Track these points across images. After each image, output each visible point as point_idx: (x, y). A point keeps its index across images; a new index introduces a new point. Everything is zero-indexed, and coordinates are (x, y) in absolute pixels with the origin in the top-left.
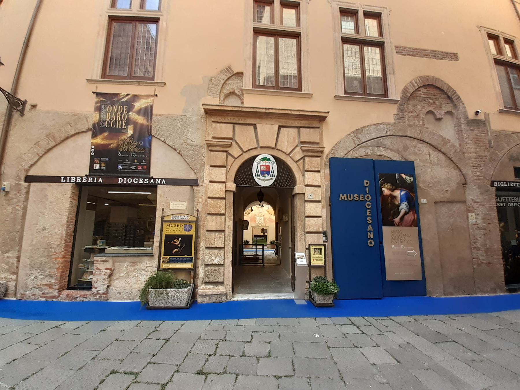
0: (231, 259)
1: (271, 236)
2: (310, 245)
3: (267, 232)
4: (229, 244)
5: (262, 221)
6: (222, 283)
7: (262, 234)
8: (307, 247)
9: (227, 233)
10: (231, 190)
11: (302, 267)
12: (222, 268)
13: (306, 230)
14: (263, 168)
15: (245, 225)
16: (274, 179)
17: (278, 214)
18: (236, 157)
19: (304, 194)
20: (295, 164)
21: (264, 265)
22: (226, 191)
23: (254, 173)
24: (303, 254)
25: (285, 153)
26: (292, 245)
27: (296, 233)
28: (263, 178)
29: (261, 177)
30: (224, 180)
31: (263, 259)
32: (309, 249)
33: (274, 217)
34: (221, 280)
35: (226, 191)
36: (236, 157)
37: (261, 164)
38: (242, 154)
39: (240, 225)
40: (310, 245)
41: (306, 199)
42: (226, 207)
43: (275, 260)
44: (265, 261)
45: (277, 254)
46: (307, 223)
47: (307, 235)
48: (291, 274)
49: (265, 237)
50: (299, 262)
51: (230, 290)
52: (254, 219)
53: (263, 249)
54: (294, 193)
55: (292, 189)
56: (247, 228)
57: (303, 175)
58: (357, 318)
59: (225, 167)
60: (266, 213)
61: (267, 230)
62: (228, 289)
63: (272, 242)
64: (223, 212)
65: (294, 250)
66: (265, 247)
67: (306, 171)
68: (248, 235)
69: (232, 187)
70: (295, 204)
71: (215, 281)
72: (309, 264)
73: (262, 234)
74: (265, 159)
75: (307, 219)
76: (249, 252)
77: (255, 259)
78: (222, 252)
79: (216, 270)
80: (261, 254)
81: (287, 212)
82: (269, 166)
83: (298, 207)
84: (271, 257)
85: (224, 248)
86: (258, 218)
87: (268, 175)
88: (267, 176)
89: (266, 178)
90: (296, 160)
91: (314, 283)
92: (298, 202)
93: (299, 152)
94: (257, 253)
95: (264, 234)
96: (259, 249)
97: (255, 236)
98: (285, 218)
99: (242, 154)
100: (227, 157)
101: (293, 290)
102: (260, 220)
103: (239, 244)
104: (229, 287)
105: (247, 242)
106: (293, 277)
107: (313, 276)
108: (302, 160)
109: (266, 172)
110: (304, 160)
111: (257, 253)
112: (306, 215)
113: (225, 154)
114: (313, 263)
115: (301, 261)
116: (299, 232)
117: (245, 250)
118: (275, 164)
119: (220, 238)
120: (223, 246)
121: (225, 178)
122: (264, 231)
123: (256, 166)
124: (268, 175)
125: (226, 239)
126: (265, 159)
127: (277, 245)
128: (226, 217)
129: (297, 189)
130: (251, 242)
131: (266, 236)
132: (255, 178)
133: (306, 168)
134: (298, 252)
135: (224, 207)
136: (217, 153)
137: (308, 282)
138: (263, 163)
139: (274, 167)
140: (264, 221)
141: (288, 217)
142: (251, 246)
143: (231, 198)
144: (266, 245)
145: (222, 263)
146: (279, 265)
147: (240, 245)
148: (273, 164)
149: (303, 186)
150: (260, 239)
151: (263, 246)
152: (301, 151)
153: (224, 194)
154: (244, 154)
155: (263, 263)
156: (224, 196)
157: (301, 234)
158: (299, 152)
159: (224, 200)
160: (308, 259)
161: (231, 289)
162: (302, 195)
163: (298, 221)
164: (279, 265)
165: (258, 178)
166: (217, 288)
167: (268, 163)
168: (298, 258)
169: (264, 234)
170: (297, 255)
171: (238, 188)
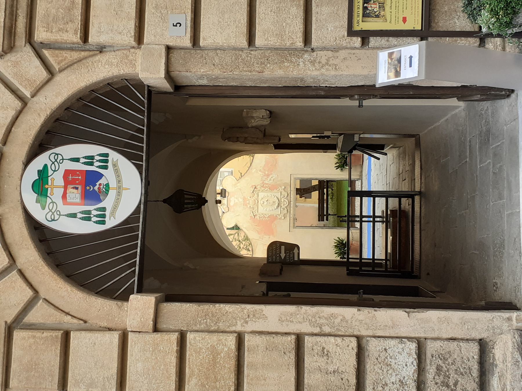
0: (399, 314)
1: (321, 165)
2: (351, 32)
3: (310, 180)
4: (344, 319)
5: (273, 196)
6: (484, 347)
7: (315, 195)
8: (357, 41)
9: (305, 328)
10: (152, 311)
11: (430, 61)
12: (431, 348)
13: (300, 44)
14: (74, 195)
15: (282, 255)
16: (114, 156)
17: (246, 141)
18: (29, 293)
19: (169, 49)
20: (58, 78)
21: (420, 193)
22: (156, 330)
23: (90, 228)
24: (383, 56)
25: (19, 113)
26: (351, 97)
27: (309, 82)
28: (112, 194)
29: (108, 203)
30: (115, 338)
31: (399, 195)
32: (365, 36)
33: (256, 155)
34: (474, 350)
35: (156, 330)
36: (29, 293)
37: (59, 201)
38: (21, 273)
39: (283, 277)
40: (351, 32)
41: (187, 42)
42: (214, 327)
43: (402, 156)
44: (405, 187)
45: (382, 147)
46: (274, 42)
47: (315, 43)
48: (453, 102)
49: (324, 185)
50: (410, 74)
51: (509, 319)
52: (266, 224)
53: (362, 194)
54: (166, 86)
55: (151, 92)
56: (292, 248)
57: (101, 49)
58: (116, 371)
59: (66, 336)
60: (246, 184)
61: (302, 181)
62: (505, 326)
63: (343, 164)
64: (231, 341)
65: (368, 91)
66: (358, 188)
67: (85, 38)
68: (318, 244)
69: (140, 306)
70: (204, 82)
71: (475, 373)
72: (422, 34)
73: (315, 195)
74: (41, 186)
75: (259, 41)
76: (375, 243)
77: (399, 223)
78: (373, 347)
79: (439, 369)
80: (380, 202)
81: (240, 111)
82: (67, 173)
83: (217, 72)
84: (393, 170)
85: (359, 338)
86: (264, 210)
87: (101, 176)
88: (102, 181)
89: (113, 184)
90: (44, 74)
91: (486, 20)
92: (197, 72)
93: (16, 64)
94: (378, 213)
95: (314, 188)
96: (365, 206)
97: (322, 216)
98: (259, 118)
99: (21, 273)
100: (31, 327)
101: (509, 93)
102: (268, 204)
103: (352, 282)
104: (497, 323)
105: (343, 246)
106: (463, 92)
107: (462, 23)
108: (46, 53)
109: (89, 185)
110: (49, 46)
111: (378, 213)
112: (244, 42)
113: (18, 335)
114: (415, 23)
115: (408, 63)
116: (308, 70)
117: (367, 254)
118: (58, 150)
119: (324, 353)
120: (354, 343)
121: (108, 335)
122: (304, 191)
123: (68, 217)
124: (101, 176)
125: (327, 329)
126: (41, 186)
127: (353, 146)
128: (249, 328)
129: (152, 74)
130: (341, 233)
131: (321, 182)
132: (111, 223)
133: (76, 38)
134: (375, 76)
135: (215, 337)
136: (14, 366)
137: (483, 40)
138: (56, 194)
139: (74, 154)
140: (272, 188)
141: (255, 108)
142: (354, 233)
143: (181, 313)
144: (352, 183)
145: (413, 346)
146: (418, 144)
147: (350, 273)
148: (58, 160)
149: (139, 53)
150: (333, 201)
151: (353, 194)
152: (11, 57)
153: (166, 336)
154: (21, 262)
155: (411, 196)
156: (174, 337)
157: (313, 62)
158: (16, 64)
159: (190, 337)
160: (401, 40)
161: (505, 314)
162: (175, 56)
163: (267, 74)
164: (418, 144)
165: (113, 213)
166: (500, 365)
167: (57, 179)
168: (397, 74)
169: (314, 188)
170: (384, 78)
171: (146, 282)
